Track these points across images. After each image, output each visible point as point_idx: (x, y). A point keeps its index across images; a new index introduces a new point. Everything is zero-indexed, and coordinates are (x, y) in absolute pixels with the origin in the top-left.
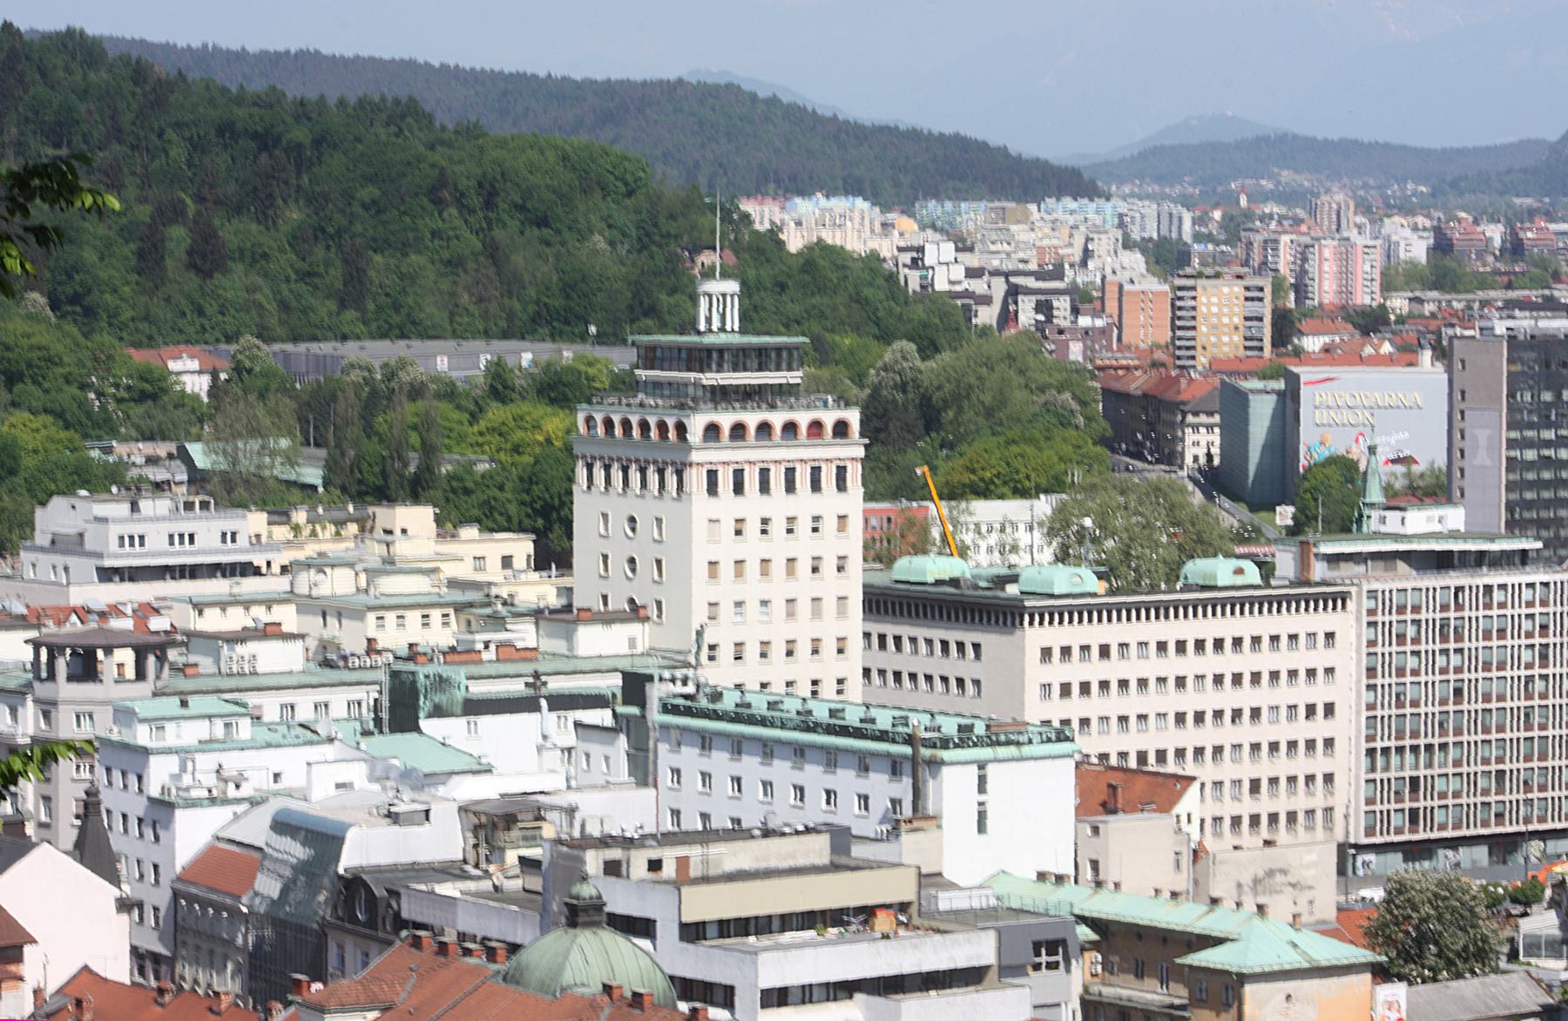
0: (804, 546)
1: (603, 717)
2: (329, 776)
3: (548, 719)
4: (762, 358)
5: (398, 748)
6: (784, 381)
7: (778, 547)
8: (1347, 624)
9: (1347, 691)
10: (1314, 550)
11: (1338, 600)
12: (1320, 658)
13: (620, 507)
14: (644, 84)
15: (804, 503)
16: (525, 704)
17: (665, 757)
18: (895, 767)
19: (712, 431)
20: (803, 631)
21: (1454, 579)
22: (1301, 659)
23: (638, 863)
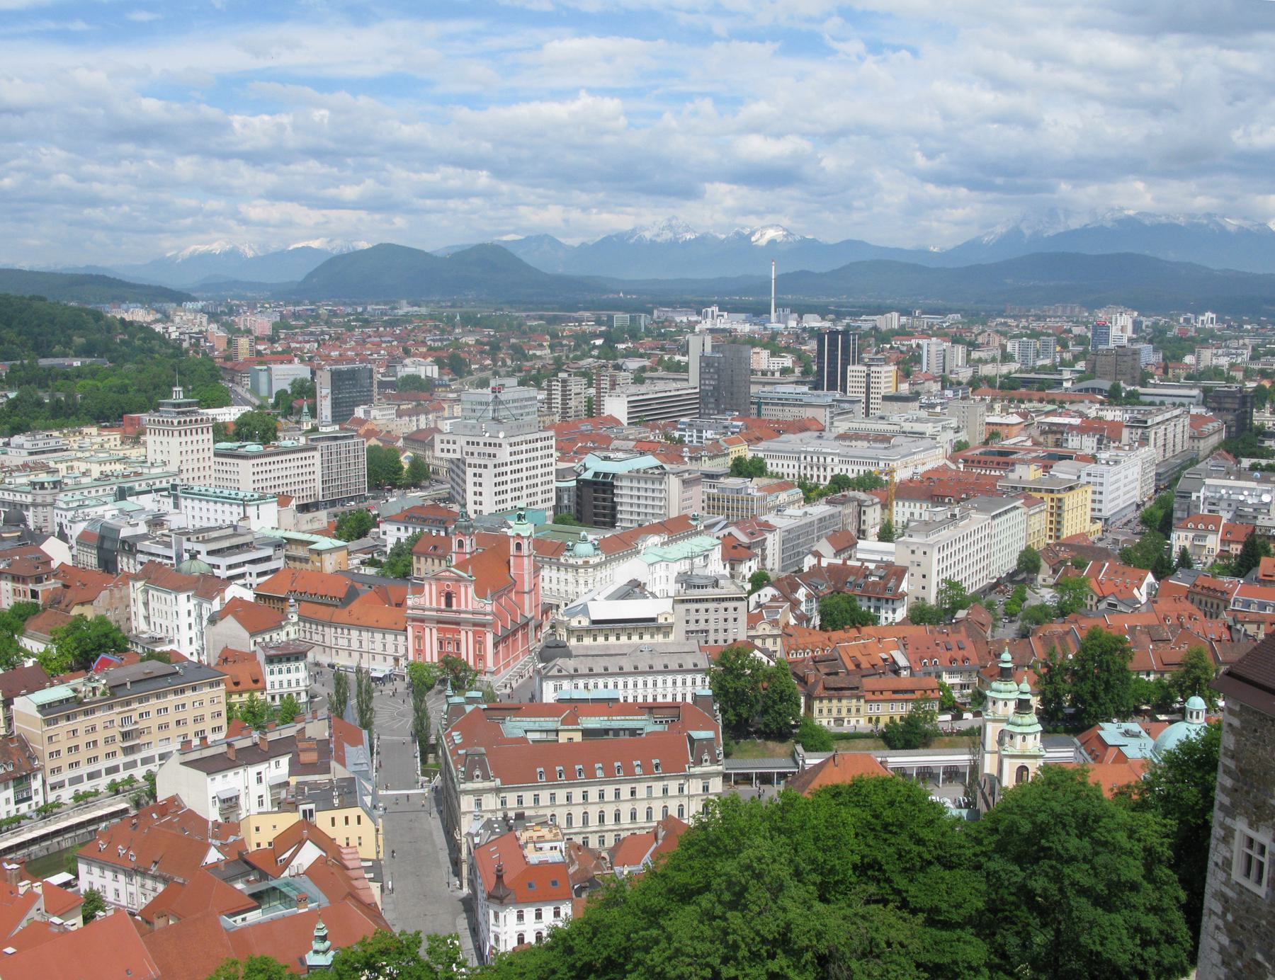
0: (201, 447)
1: (165, 493)
2: (108, 512)
3: (154, 495)
4: (189, 405)
5: (121, 504)
6: (766, 760)
7: (195, 447)
8: (317, 454)
9: (318, 468)
10: (799, 748)
11: (315, 449)
12: (311, 462)
13: (158, 439)
14: (31, 272)
15: (200, 437)
16: (149, 492)
17: (183, 502)
18: (239, 505)
19: (179, 422)
20: (201, 465)
21: (339, 442)
22: (307, 462)
23: (193, 538)
